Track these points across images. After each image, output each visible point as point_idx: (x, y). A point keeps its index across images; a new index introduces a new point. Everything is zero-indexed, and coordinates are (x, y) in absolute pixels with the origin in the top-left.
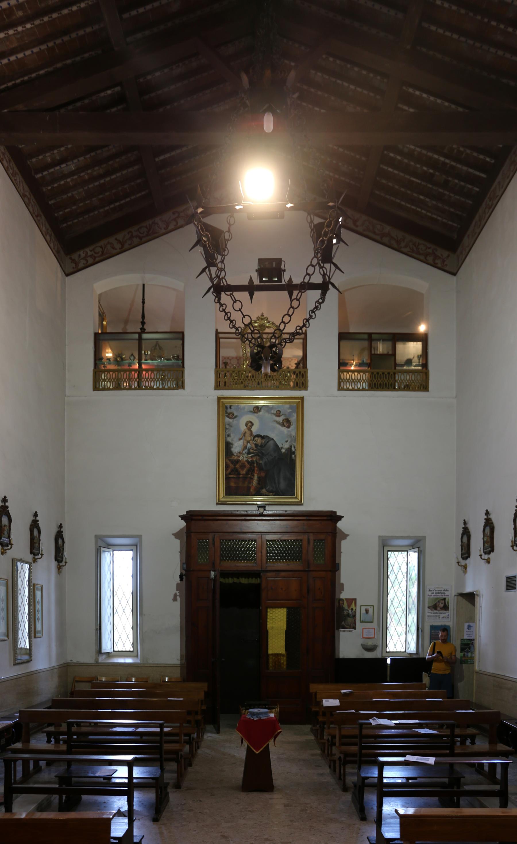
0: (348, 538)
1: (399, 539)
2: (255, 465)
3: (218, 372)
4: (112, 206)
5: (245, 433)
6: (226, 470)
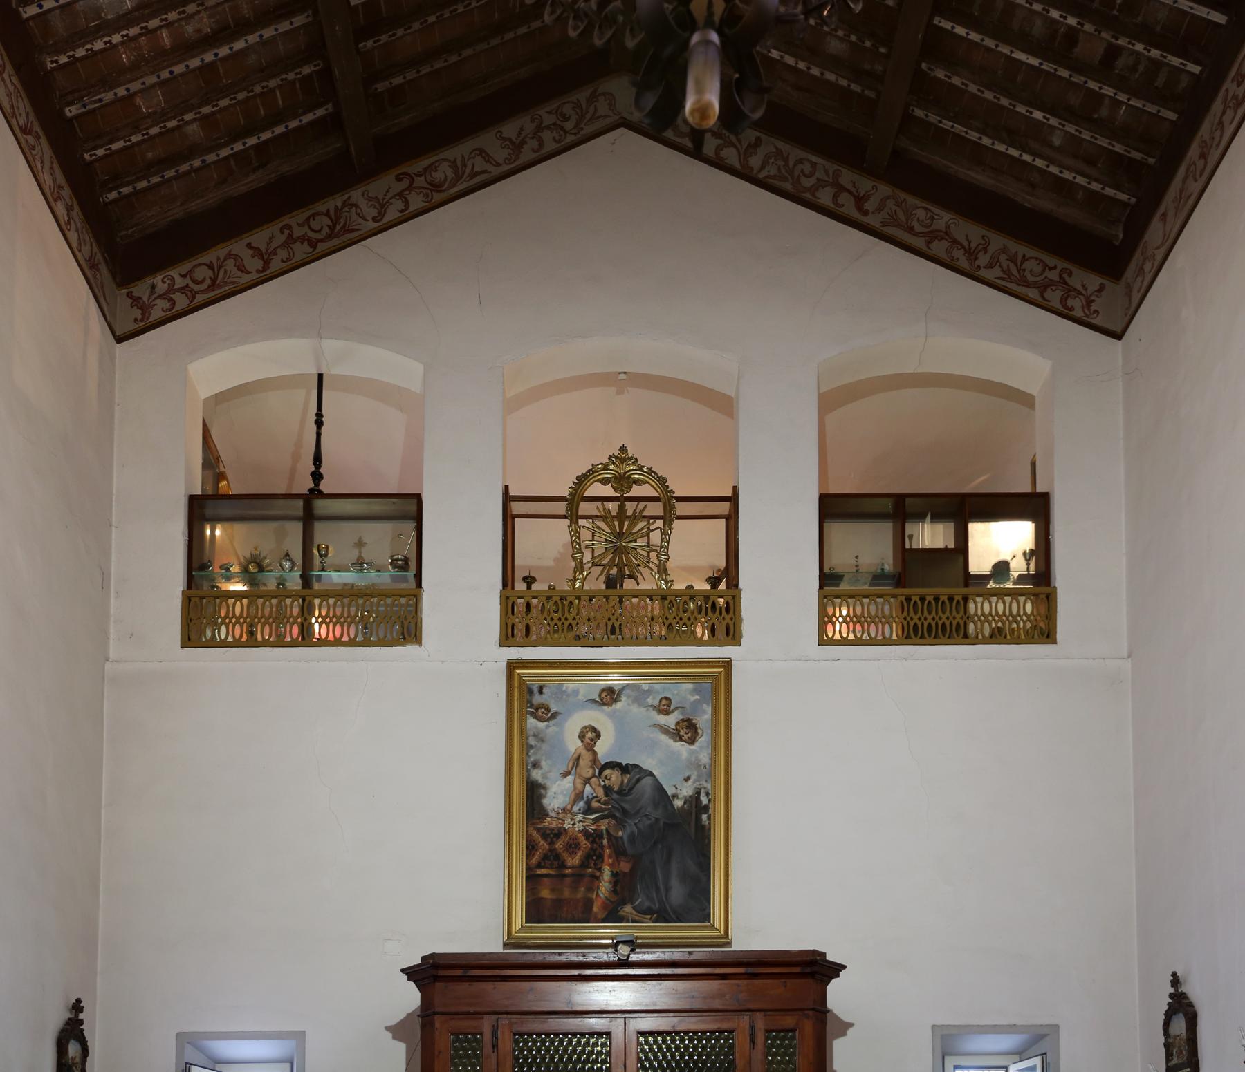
0: (850, 1032)
1: (986, 1033)
2: (605, 842)
3: (512, 599)
4: (238, 147)
5: (578, 759)
6: (529, 856)
